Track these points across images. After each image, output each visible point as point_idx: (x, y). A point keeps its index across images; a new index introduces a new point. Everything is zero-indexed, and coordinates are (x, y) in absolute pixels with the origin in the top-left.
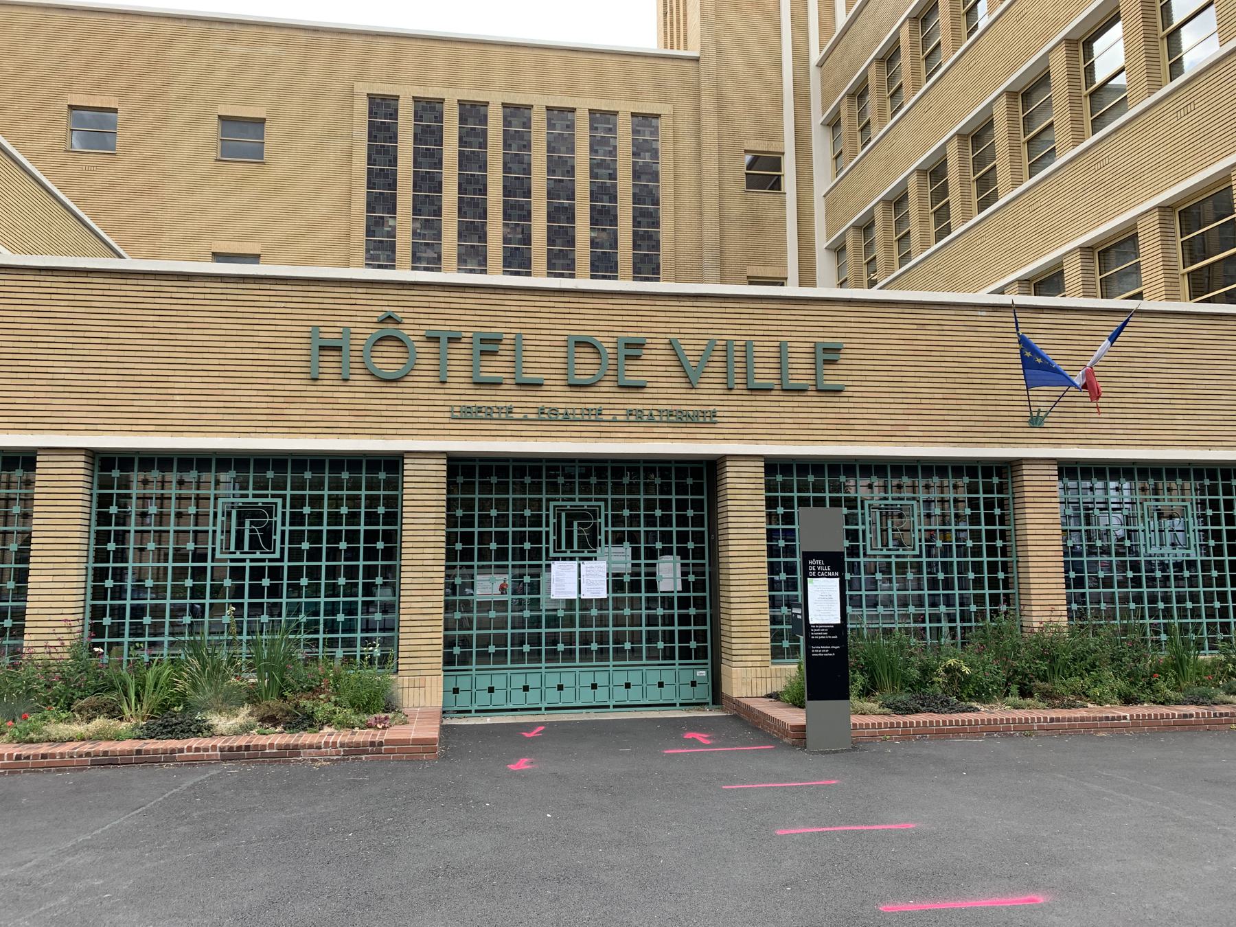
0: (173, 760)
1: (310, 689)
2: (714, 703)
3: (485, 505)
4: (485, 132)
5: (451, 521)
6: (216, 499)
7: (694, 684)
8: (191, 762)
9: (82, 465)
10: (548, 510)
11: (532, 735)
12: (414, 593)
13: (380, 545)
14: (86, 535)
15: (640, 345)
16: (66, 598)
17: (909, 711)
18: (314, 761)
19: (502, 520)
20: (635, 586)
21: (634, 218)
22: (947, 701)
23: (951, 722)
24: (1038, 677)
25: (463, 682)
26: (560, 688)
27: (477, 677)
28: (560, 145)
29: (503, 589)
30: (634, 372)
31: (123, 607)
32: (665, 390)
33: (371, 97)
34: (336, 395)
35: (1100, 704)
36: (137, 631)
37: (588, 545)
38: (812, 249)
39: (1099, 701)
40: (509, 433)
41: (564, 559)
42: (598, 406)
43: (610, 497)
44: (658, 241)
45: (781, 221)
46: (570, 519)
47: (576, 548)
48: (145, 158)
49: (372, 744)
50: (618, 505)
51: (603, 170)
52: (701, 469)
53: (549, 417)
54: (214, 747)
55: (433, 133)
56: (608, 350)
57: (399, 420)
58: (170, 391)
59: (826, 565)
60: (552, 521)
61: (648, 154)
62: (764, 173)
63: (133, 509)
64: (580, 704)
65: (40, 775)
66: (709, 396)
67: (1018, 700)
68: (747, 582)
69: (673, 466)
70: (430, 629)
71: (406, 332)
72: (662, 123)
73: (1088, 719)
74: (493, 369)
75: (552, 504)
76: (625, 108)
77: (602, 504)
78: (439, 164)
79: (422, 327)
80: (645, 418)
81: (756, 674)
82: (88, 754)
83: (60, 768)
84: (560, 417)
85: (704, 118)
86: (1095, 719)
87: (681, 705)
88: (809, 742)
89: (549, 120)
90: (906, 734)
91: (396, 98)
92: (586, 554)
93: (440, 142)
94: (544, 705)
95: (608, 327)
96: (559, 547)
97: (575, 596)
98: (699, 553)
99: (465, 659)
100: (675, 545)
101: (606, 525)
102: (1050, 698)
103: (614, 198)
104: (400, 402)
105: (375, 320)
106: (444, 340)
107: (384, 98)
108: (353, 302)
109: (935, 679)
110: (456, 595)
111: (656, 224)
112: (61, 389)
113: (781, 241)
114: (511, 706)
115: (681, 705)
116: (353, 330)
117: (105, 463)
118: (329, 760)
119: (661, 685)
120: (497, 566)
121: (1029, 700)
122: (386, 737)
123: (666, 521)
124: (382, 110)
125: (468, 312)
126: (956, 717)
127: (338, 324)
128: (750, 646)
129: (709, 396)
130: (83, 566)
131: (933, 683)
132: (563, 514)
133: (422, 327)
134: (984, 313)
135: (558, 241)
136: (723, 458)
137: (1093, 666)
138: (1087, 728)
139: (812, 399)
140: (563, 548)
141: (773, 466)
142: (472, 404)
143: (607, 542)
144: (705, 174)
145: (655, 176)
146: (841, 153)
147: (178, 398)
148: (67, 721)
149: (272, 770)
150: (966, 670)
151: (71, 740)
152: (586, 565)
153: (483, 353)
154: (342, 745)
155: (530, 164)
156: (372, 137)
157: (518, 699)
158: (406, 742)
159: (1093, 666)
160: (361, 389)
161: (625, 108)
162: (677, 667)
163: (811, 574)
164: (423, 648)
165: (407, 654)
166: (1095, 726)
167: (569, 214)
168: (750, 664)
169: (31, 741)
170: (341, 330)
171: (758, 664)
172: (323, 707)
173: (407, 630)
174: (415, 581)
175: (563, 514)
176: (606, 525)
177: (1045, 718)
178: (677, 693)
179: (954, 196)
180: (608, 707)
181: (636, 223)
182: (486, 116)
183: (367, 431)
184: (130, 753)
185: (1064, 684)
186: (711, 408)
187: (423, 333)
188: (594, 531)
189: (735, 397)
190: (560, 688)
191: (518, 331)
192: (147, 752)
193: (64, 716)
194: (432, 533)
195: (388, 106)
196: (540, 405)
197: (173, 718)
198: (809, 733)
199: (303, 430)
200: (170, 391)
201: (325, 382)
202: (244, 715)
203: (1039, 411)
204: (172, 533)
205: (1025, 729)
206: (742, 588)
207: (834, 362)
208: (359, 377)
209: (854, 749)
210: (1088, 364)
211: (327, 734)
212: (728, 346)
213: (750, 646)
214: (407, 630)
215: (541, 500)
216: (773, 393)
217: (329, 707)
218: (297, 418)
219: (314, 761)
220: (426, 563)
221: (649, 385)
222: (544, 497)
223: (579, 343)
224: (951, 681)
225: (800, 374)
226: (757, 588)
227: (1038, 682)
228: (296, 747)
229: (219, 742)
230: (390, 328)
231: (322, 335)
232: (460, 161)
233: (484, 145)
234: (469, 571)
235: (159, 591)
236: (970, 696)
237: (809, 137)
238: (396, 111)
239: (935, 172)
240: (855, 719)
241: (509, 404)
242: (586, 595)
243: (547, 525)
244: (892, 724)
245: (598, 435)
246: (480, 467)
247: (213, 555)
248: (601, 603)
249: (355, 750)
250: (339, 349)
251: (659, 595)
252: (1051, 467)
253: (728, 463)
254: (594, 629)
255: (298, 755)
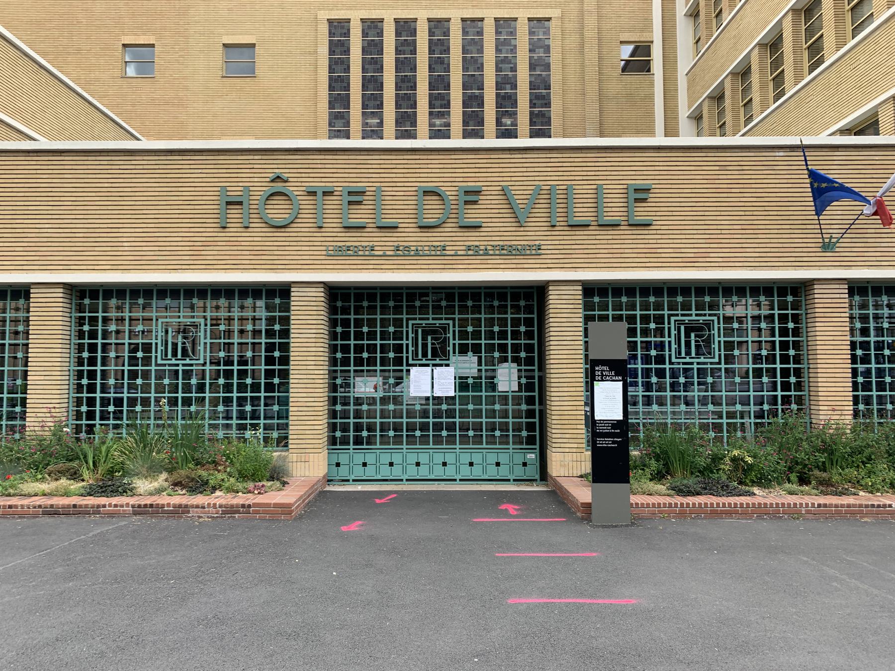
0: (99, 513)
1: (214, 462)
2: (541, 480)
3: (358, 323)
4: (415, 41)
5: (333, 336)
6: (157, 320)
7: (525, 464)
8: (111, 515)
9: (61, 295)
11: (383, 501)
12: (300, 390)
13: (277, 354)
14: (810, 348)
15: (478, 192)
16: (54, 392)
17: (690, 493)
18: (200, 517)
19: (372, 335)
20: (477, 387)
21: (531, 101)
22: (727, 486)
23: (724, 504)
24: (818, 467)
25: (343, 458)
26: (444, 464)
27: (353, 456)
28: (473, 46)
30: (472, 215)
31: (122, 399)
32: (497, 227)
33: (330, 21)
35: (871, 492)
36: (104, 416)
37: (438, 354)
38: (676, 118)
39: (872, 490)
41: (421, 365)
42: (442, 244)
43: (457, 316)
44: (550, 118)
45: (651, 97)
47: (430, 357)
48: (175, 79)
49: (243, 506)
50: (463, 323)
51: (506, 64)
53: (403, 253)
54: (127, 505)
55: (376, 45)
56: (451, 198)
57: (287, 257)
58: (120, 239)
59: (611, 370)
61: (542, 50)
62: (638, 62)
64: (433, 477)
65: (6, 520)
67: (795, 487)
69: (509, 291)
72: (553, 24)
73: (854, 506)
74: (359, 216)
75: (411, 322)
76: (522, 15)
78: (381, 69)
79: (303, 184)
80: (481, 252)
81: (570, 460)
82: (40, 506)
83: (21, 516)
84: (412, 253)
85: (586, 17)
86: (860, 506)
87: (514, 480)
88: (593, 516)
89: (463, 29)
90: (683, 513)
91: (348, 21)
92: (438, 362)
93: (381, 52)
94: (405, 477)
95: (450, 179)
98: (529, 361)
99: (345, 441)
101: (454, 339)
102: (826, 486)
103: (514, 86)
104: (287, 244)
105: (268, 180)
106: (320, 194)
107: (340, 21)
108: (251, 166)
109: (722, 466)
111: (548, 105)
112: (45, 240)
113: (651, 114)
114: (379, 477)
115: (514, 480)
116: (251, 189)
117: (81, 295)
118: (211, 517)
119: (498, 464)
120: (367, 371)
121: (806, 488)
122: (256, 501)
123: (503, 335)
124: (338, 29)
125: (339, 171)
126: (733, 500)
127: (241, 184)
128: (567, 436)
130: (66, 369)
131: (718, 470)
132: (420, 331)
133: (303, 184)
134: (781, 154)
135: (471, 123)
136: (548, 283)
137: (869, 459)
138: (852, 514)
139: (625, 233)
140: (420, 357)
142: (343, 244)
143: (454, 352)
144: (587, 62)
145: (547, 67)
146: (699, 39)
147: (125, 244)
148: (43, 480)
149: (165, 523)
150: (749, 460)
151: (36, 495)
152: (437, 370)
153: (350, 203)
154: (221, 506)
155: (449, 65)
156: (331, 52)
157: (385, 472)
158: (268, 505)
159: (869, 459)
160: (258, 234)
161: (522, 15)
164: (307, 432)
165: (295, 437)
166: (861, 512)
167: (480, 101)
168: (567, 450)
169: (9, 495)
171: (574, 450)
173: (295, 418)
174: (301, 381)
175: (420, 331)
177: (813, 504)
178: (511, 470)
179: (788, 66)
180: (455, 480)
181: (532, 105)
182: (415, 29)
183: (263, 267)
184: (69, 506)
185: (840, 474)
186: (537, 243)
187: (304, 189)
188: (445, 342)
189: (557, 233)
190: (418, 464)
191: (378, 184)
192: (81, 506)
193: (40, 476)
194: (313, 345)
195: (343, 27)
196: (396, 244)
197: (112, 483)
199: (215, 267)
200: (120, 239)
202: (162, 479)
203: (831, 238)
205: (793, 513)
207: (644, 200)
208: (256, 225)
209: (633, 524)
210: (878, 194)
211: (220, 498)
212: (551, 191)
213: (567, 436)
214: (295, 418)
216: (590, 228)
217: (220, 476)
219: (200, 517)
220: (309, 367)
221: (484, 225)
223: (426, 193)
224: (736, 469)
225: (615, 211)
226: (574, 389)
227: (817, 472)
228: (186, 506)
229: (132, 501)
230: (278, 186)
231: (229, 193)
232: (396, 66)
233: (414, 52)
234: (398, 374)
235: (119, 388)
236: (753, 482)
237: (674, 26)
238: (349, 30)
239: (773, 45)
240: (634, 499)
242: (437, 394)
243: (407, 339)
244: (670, 504)
245: (443, 266)
246: (381, 294)
247: (156, 361)
248: (450, 400)
249: (230, 510)
250: (240, 203)
252: (842, 286)
253: (550, 288)
254: (418, 420)
255: (188, 512)
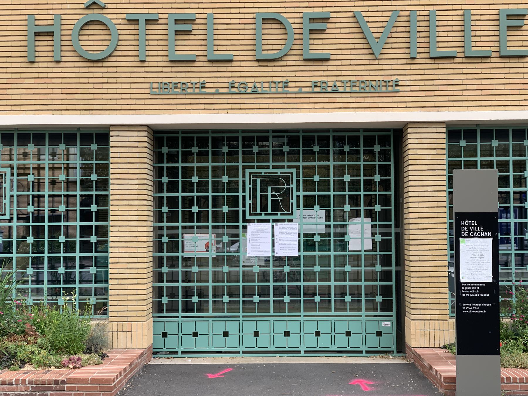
1: (22, 332)
2: (398, 352)
5: (159, 187)
7: (379, 334)
10: (244, 176)
15: (325, 20)
20: (325, 245)
25: (171, 327)
29: (207, 247)
30: (319, 46)
32: (348, 61)
34: (50, 75)
37: (280, 208)
40: (202, 107)
41: (259, 221)
42: (284, 79)
46: (264, 184)
47: (270, 211)
49: (56, 382)
52: (389, 136)
53: (238, 91)
56: (294, 26)
57: (105, 96)
59: (479, 225)
60: (248, 186)
63: (46, 177)
66: (392, 66)
68: (427, 242)
70: (135, 281)
71: (109, 16)
74: (187, 48)
75: (247, 171)
77: (294, 171)
79: (123, 11)
87: (367, 352)
92: (279, 216)
96: (255, 209)
97: (269, 254)
99: (172, 308)
100: (362, 208)
106: (142, 22)
110: (166, 250)
114: (212, 349)
115: (367, 352)
116: (64, 17)
120: (198, 227)
123: (354, 185)
127: (51, 12)
128: (428, 301)
129: (392, 66)
132: (258, 181)
133: (123, 11)
139: (496, 66)
140: (259, 211)
141: (455, 132)
142: (169, 80)
143: (298, 206)
152: (279, 226)
154: (30, 383)
157: (219, 343)
160: (71, 70)
162: (364, 318)
163: (463, 234)
164: (130, 298)
168: (428, 317)
170: (26, 17)
171: (436, 317)
172: (25, 349)
173: (116, 282)
175: (258, 181)
176: (12, 190)
178: (364, 341)
180: (299, 352)
186: (394, 78)
187: (124, 16)
188: (288, 193)
189: (418, 66)
191: (210, 11)
194: (135, 197)
196: (230, 80)
198: (459, 386)
199: (23, 108)
201: (41, 65)
204: (47, 197)
206: (421, 247)
207: (518, 28)
208: (69, 59)
211: (30, 373)
213: (428, 301)
214: (116, 282)
215: (237, 168)
216: (456, 60)
217: (30, 348)
218: (18, 97)
221: (332, 57)
222: (240, 164)
223: (265, 20)
226: (436, 247)
230: (94, 14)
231: (37, 23)
234: (233, 231)
240: (505, 373)
241: (202, 80)
242: (279, 253)
245: (285, 106)
248: (293, 260)
250: (51, 34)
251: (347, 253)
253: (410, 130)
254: (256, 284)
